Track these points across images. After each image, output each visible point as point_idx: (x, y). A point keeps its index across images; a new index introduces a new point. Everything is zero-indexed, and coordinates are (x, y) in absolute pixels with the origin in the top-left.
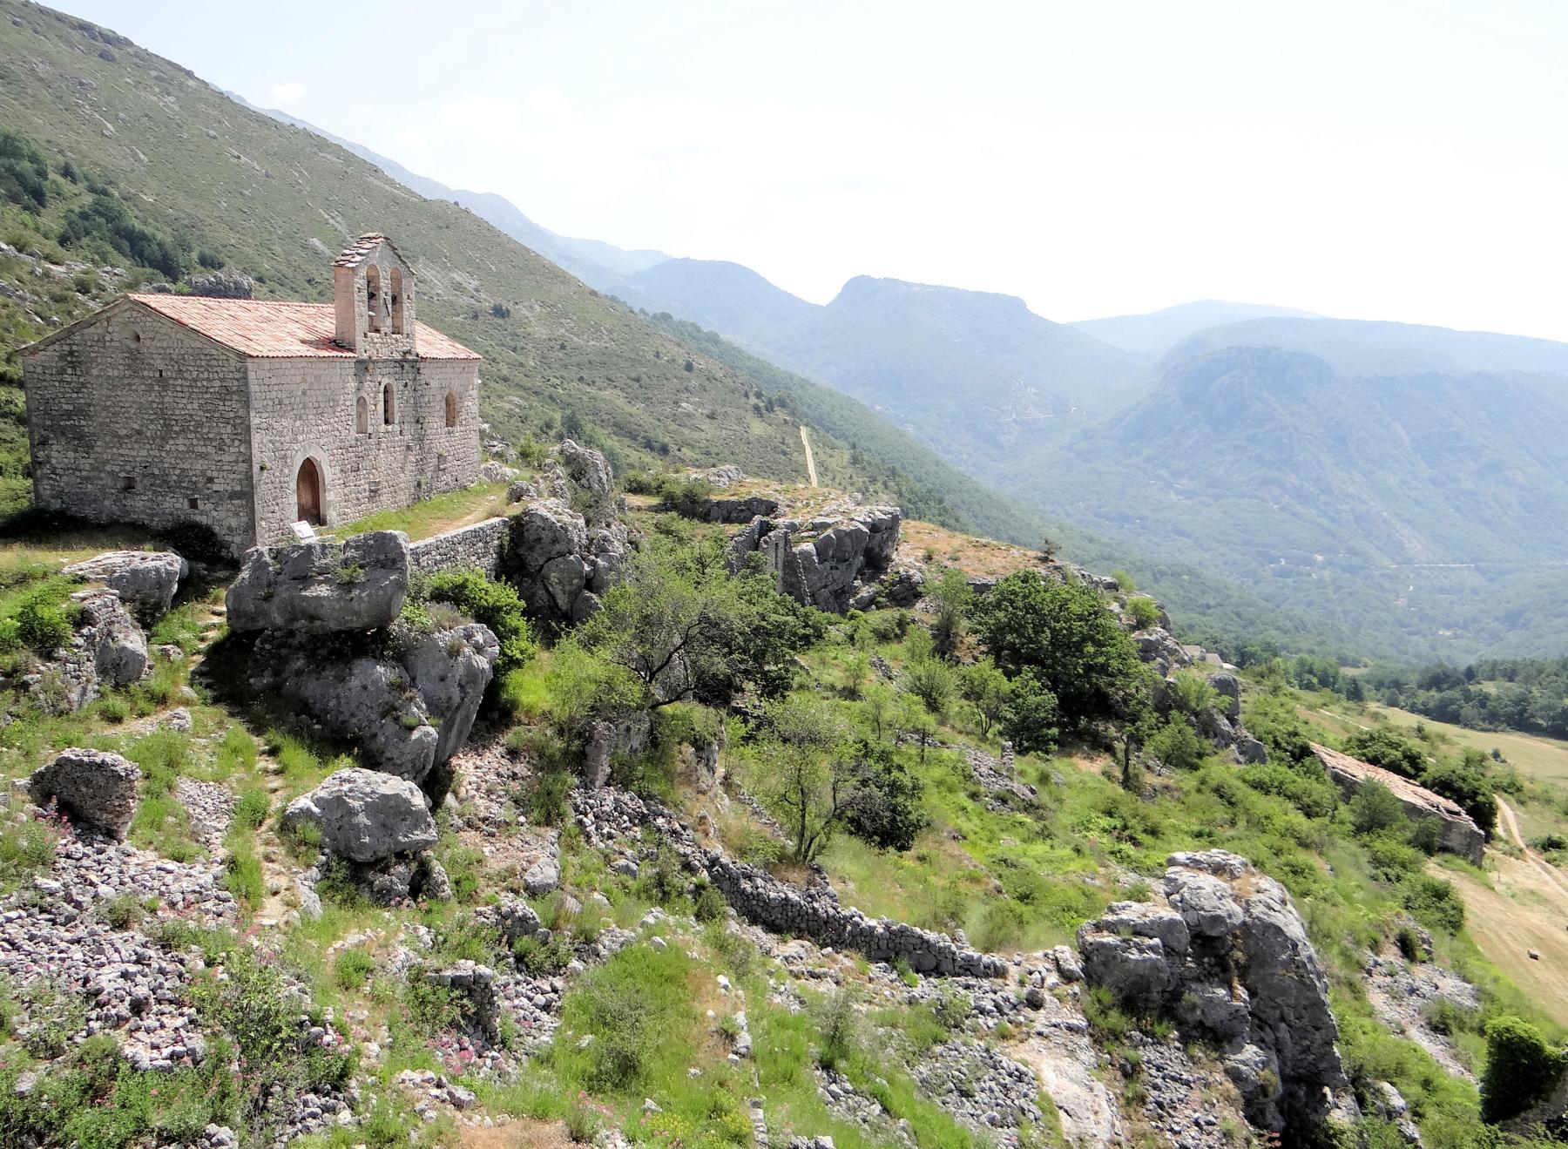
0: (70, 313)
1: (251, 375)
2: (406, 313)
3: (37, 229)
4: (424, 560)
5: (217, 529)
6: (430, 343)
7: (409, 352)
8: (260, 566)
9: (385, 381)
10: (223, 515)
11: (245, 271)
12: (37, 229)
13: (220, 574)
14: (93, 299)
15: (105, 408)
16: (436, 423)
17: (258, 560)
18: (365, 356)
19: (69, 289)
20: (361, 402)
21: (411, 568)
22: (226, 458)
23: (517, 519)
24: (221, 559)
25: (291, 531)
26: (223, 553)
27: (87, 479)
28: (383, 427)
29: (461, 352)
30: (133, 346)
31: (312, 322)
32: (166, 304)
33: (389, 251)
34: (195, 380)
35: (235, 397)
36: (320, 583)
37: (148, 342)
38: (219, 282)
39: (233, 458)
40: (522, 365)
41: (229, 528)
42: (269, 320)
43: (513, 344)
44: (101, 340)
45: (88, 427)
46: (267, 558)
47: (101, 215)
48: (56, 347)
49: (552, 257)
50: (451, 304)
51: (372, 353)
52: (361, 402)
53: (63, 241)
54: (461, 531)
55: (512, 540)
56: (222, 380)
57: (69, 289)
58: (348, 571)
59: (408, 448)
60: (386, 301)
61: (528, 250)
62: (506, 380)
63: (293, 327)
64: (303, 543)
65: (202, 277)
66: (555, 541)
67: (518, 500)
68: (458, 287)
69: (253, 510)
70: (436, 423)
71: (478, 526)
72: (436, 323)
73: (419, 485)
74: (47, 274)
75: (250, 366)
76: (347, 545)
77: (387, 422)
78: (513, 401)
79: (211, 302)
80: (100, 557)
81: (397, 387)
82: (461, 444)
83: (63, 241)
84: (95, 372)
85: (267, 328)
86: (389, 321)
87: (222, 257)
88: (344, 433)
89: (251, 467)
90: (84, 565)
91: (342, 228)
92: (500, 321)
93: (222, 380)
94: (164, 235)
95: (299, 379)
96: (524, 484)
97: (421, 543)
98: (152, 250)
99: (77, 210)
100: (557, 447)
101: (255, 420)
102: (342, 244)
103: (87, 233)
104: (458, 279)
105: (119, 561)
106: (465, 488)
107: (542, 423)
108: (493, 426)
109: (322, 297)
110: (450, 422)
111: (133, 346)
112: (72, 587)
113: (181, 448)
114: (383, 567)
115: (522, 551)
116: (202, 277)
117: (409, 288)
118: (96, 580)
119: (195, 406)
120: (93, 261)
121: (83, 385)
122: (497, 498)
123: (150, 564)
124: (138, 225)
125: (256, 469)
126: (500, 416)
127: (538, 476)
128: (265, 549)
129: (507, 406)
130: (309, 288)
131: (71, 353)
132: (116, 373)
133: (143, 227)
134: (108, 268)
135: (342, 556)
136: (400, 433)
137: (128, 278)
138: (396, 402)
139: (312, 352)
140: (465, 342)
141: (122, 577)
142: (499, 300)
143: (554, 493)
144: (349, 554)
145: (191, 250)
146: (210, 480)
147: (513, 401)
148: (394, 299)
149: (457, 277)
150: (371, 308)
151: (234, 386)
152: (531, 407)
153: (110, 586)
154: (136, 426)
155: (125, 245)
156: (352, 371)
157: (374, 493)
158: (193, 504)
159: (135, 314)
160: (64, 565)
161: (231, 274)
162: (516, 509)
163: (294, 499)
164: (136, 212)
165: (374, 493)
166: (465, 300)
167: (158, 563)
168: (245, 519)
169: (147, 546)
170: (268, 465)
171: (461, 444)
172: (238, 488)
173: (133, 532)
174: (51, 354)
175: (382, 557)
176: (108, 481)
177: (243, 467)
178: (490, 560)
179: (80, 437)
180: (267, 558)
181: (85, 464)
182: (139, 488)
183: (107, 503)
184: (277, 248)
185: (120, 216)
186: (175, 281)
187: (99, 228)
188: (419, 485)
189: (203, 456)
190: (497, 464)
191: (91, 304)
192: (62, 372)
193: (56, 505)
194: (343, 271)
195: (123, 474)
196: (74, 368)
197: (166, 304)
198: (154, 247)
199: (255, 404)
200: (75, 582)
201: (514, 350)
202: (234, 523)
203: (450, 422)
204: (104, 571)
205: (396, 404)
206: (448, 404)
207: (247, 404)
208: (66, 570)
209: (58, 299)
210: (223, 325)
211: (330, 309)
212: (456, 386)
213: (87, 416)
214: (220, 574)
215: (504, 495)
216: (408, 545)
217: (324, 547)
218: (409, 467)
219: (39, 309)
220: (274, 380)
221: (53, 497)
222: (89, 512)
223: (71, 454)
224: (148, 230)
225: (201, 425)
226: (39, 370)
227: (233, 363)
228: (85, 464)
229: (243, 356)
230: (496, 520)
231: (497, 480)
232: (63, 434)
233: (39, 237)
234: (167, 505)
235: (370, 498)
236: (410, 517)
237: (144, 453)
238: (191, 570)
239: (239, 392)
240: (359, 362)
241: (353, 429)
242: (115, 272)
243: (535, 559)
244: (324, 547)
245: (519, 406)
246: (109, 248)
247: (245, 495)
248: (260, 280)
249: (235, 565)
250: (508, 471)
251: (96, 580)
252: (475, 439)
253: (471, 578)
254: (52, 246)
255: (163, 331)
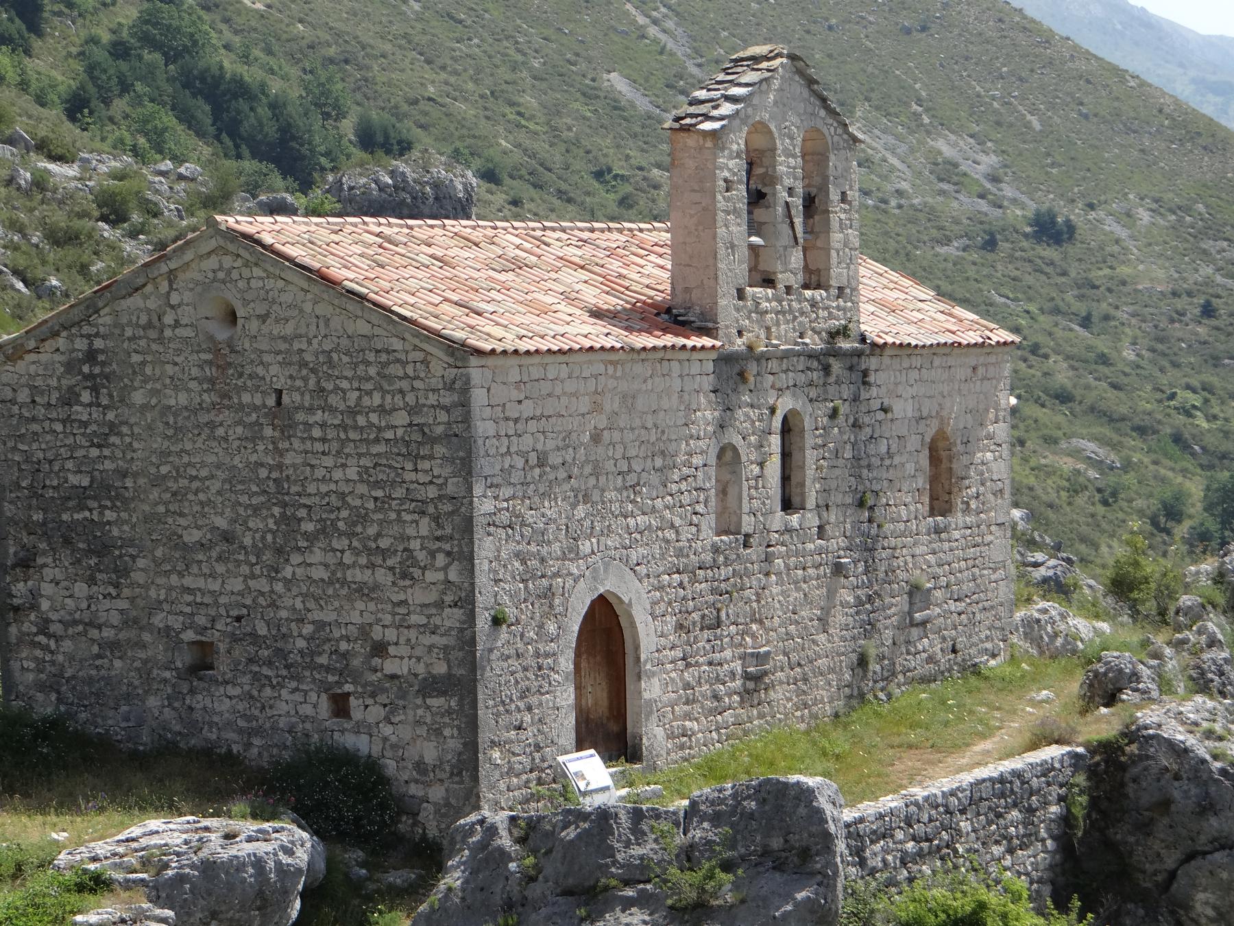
0: (84, 269)
1: (478, 397)
2: (836, 237)
3: (23, 85)
4: (875, 852)
5: (390, 766)
6: (895, 308)
7: (843, 332)
8: (489, 859)
9: (786, 404)
10: (405, 733)
11: (456, 155)
12: (23, 85)
13: (396, 878)
14: (133, 234)
15: (158, 481)
16: (904, 505)
17: (484, 845)
18: (739, 344)
19: (83, 215)
20: (728, 457)
21: (848, 872)
22: (418, 596)
23: (1107, 750)
24: (400, 839)
25: (560, 775)
26: (404, 825)
27: (114, 645)
28: (778, 519)
29: (968, 327)
30: (222, 335)
31: (615, 265)
32: (292, 234)
33: (798, 88)
34: (353, 412)
35: (440, 450)
36: (627, 904)
37: (254, 325)
38: (401, 184)
39: (432, 597)
40: (1104, 359)
41: (420, 766)
42: (518, 266)
43: (1081, 308)
44: (154, 324)
45: (119, 524)
46: (505, 841)
47: (155, 45)
48: (61, 342)
49: (1180, 86)
50: (932, 214)
51: (755, 335)
52: (728, 457)
53: (76, 107)
54: (967, 778)
55: (1094, 803)
56: (413, 410)
57: (83, 215)
58: (696, 877)
59: (838, 569)
60: (793, 212)
61: (1119, 73)
62: (1063, 397)
63: (572, 278)
64: (589, 804)
65: (360, 176)
66: (1207, 807)
67: (1111, 699)
68: (948, 172)
69: (472, 724)
70: (904, 505)
71: (1007, 766)
72: (899, 258)
73: (863, 662)
74: (40, 183)
75: (476, 375)
76: (693, 811)
77: (787, 505)
78: (1084, 450)
79: (392, 227)
80: (135, 831)
81: (813, 418)
82: (971, 558)
83: (76, 107)
84: (138, 398)
85: (519, 287)
86: (796, 258)
87: (407, 128)
88: (687, 533)
89: (471, 617)
90: (101, 848)
91: (678, 47)
92: (1050, 253)
93: (413, 410)
94: (285, 84)
95: (584, 405)
96: (1124, 659)
97: (868, 808)
98: (258, 118)
99: (106, 37)
100: (1208, 566)
101: (484, 506)
102: (677, 84)
103: (125, 88)
104: (948, 151)
105: (177, 840)
106: (976, 670)
107: (1154, 505)
108: (1032, 517)
109: (626, 208)
110: (940, 503)
111: (222, 335)
112: (74, 898)
113: (319, 573)
114: (779, 867)
115: (1120, 834)
116: (360, 176)
117: (845, 176)
118: (128, 885)
119: (352, 473)
120: (135, 151)
121: (113, 428)
122: (1054, 696)
123: (243, 849)
124: (231, 65)
125: (483, 622)
126: (1048, 490)
127: (1159, 639)
128: (500, 818)
129: (1067, 464)
130: (612, 194)
131: (91, 356)
132: (183, 399)
133: (242, 69)
134: (167, 165)
135: (680, 839)
136: (814, 536)
137: (207, 184)
138: (810, 456)
139: (613, 337)
140: (986, 309)
141: (180, 879)
142: (1049, 201)
143: (1201, 685)
144: (697, 834)
145: (341, 115)
146: (380, 649)
147: (1084, 450)
148: (810, 203)
149: (945, 147)
150: (754, 227)
151: (439, 423)
152: (1127, 466)
153: (156, 900)
154: (221, 523)
155: (203, 110)
156: (708, 382)
157: (755, 683)
158: (340, 707)
159: (228, 261)
160: (58, 846)
161: (434, 165)
162: (1104, 724)
163: (567, 696)
164: (228, 35)
165: (755, 683)
166: (964, 205)
167: (262, 848)
168: (454, 744)
169: (239, 807)
170: (511, 612)
171: (971, 558)
172: (441, 669)
173: (201, 773)
174: (51, 356)
175: (776, 843)
176: (158, 651)
177: (452, 618)
178: (1038, 856)
179: (102, 549)
180: (505, 841)
181: (111, 611)
182: (223, 666)
183: (153, 702)
184: (529, 101)
185: (195, 45)
186: (305, 186)
187: (149, 76)
188: (863, 662)
189: (365, 591)
190: (1053, 607)
191: (128, 246)
192: (70, 399)
193: (45, 706)
194: (691, 141)
195: (189, 636)
196: (95, 390)
197: (292, 234)
198: (263, 111)
199: (485, 465)
200: (81, 888)
201: (1086, 322)
202: (430, 753)
203: (940, 503)
204: (145, 863)
205: (810, 459)
206: (935, 459)
207: (466, 468)
208: (63, 858)
209: (60, 238)
210: (417, 279)
211: (660, 234)
212: (955, 413)
213: (119, 500)
214: (396, 878)
215: (1075, 686)
216: (843, 816)
217: (637, 815)
218: (839, 618)
219: (22, 262)
220: (528, 409)
221: (42, 687)
222: (114, 723)
223: (81, 589)
224: (251, 75)
225: (362, 518)
226: (23, 396)
227: (437, 368)
228: (111, 611)
229: (461, 352)
230: (1052, 752)
231: (1053, 651)
232: (67, 542)
233: (26, 102)
234: (283, 707)
235: (747, 695)
236: (840, 741)
237: (236, 584)
238: (330, 862)
239: (448, 437)
240: (726, 360)
241: (708, 524)
242: (176, 175)
243: (1155, 854)
244: (637, 815)
245: (1098, 464)
246: (168, 119)
247: (459, 684)
248: (490, 176)
249: (431, 858)
250: (1081, 625)
251: (128, 885)
252: (1000, 547)
253: (992, 898)
254: (52, 121)
255: (287, 298)
